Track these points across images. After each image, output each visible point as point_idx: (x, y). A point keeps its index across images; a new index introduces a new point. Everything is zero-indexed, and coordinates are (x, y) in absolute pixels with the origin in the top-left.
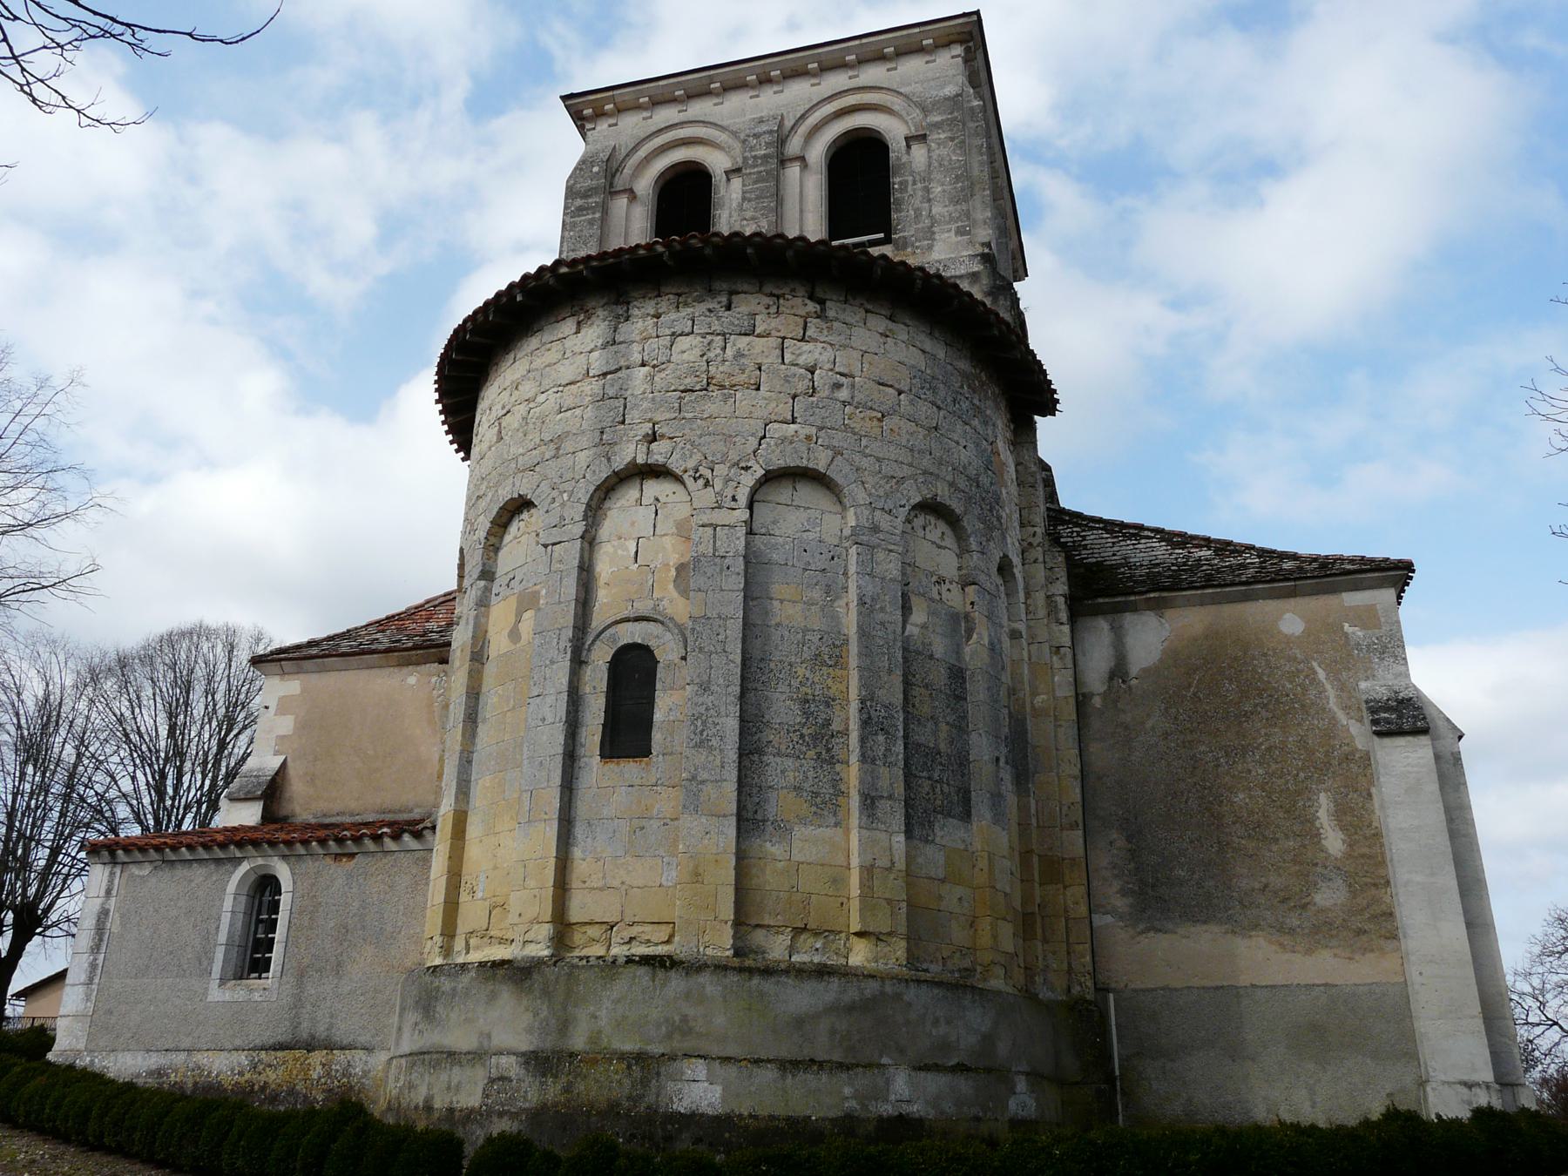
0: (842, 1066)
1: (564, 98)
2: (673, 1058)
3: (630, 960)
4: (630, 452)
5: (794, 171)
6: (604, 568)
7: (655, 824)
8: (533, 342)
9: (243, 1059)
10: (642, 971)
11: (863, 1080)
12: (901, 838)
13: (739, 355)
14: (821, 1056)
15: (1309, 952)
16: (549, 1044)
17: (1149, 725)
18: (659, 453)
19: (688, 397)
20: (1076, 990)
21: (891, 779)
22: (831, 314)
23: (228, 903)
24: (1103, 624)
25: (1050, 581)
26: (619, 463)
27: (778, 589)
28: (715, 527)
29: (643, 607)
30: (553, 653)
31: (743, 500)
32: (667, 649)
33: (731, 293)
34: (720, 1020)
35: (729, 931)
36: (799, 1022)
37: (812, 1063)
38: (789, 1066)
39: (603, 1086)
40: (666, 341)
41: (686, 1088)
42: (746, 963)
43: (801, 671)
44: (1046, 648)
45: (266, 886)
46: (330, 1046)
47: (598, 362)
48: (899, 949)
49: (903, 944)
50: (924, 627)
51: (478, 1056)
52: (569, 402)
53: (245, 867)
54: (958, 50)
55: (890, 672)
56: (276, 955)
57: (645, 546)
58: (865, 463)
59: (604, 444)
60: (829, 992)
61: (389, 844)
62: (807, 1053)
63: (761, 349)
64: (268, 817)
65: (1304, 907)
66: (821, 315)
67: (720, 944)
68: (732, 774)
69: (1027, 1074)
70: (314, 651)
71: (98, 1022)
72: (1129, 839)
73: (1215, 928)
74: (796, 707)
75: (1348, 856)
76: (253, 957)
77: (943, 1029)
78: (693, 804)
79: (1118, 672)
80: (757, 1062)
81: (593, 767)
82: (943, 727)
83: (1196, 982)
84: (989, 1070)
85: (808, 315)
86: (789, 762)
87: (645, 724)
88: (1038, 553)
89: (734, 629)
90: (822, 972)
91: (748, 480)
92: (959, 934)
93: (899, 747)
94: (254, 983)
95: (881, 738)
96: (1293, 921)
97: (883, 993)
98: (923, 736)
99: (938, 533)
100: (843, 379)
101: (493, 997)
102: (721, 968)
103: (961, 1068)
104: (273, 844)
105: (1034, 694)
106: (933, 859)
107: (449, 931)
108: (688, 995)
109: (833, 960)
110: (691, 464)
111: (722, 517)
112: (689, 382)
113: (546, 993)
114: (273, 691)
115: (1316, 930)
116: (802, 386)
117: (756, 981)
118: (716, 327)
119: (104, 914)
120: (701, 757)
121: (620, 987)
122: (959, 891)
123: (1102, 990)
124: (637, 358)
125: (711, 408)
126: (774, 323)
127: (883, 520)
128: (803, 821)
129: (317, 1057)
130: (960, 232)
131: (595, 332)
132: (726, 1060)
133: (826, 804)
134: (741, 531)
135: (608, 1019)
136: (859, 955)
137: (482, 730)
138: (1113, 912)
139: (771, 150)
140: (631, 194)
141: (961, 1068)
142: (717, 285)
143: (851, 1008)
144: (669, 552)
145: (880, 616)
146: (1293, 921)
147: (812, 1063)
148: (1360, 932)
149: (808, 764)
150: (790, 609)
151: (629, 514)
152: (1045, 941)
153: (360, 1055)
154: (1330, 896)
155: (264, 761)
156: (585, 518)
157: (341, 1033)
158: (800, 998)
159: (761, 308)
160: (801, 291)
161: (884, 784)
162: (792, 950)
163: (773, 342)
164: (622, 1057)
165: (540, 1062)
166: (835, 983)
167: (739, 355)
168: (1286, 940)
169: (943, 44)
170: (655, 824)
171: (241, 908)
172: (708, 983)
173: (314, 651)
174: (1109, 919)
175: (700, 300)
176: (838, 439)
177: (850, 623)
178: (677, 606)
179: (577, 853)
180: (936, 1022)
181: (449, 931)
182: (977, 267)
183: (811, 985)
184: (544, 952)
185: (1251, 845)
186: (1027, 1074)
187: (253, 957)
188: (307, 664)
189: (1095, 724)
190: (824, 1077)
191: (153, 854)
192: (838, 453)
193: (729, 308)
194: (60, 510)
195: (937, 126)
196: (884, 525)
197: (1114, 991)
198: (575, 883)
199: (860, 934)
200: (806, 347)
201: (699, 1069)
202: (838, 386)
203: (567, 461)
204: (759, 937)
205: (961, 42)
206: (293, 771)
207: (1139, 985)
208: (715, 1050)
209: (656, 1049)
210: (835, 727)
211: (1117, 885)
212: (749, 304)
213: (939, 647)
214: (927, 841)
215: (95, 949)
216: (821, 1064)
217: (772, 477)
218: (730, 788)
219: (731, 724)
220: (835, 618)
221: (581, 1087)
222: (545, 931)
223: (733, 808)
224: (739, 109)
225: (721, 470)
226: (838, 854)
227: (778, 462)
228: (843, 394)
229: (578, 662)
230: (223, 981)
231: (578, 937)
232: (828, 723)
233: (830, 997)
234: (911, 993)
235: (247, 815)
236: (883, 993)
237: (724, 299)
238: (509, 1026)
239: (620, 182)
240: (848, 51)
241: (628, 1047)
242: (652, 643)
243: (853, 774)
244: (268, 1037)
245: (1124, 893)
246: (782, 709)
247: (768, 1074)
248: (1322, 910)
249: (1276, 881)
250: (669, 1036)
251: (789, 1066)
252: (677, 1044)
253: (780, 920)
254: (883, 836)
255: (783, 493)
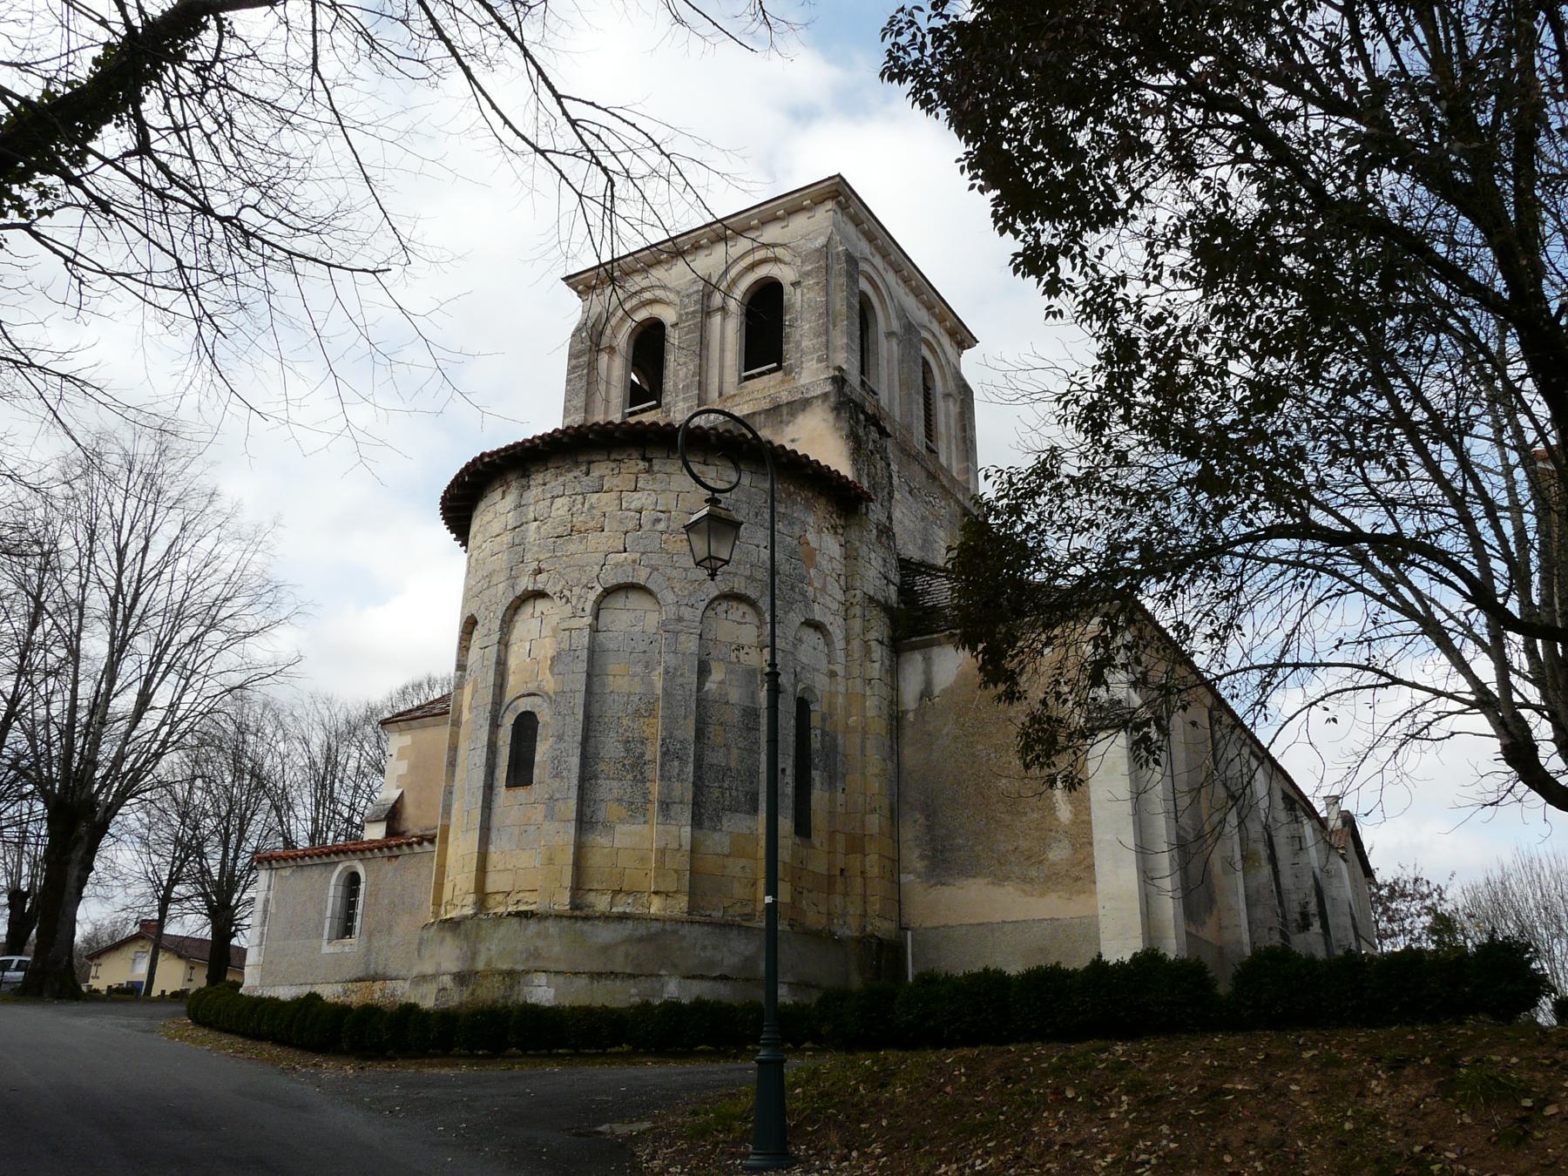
0: (632, 976)
1: (566, 279)
2: (528, 972)
3: (509, 914)
4: (525, 583)
5: (717, 319)
6: (513, 662)
7: (533, 828)
8: (482, 505)
9: (339, 988)
10: (515, 920)
11: (645, 985)
12: (689, 829)
13: (592, 507)
14: (618, 969)
15: (1042, 895)
16: (465, 968)
17: (945, 731)
18: (541, 582)
19: (560, 541)
20: (869, 929)
21: (683, 790)
22: (656, 468)
23: (331, 893)
24: (918, 657)
25: (866, 630)
26: (519, 591)
27: (612, 668)
28: (570, 630)
29: (532, 687)
30: (481, 721)
31: (589, 607)
32: (544, 716)
33: (590, 463)
34: (557, 949)
35: (568, 894)
36: (605, 949)
37: (613, 975)
38: (596, 976)
39: (490, 992)
40: (547, 503)
41: (534, 990)
42: (579, 912)
43: (625, 722)
44: (858, 681)
45: (353, 880)
46: (385, 978)
47: (511, 520)
48: (682, 903)
49: (686, 898)
50: (722, 682)
51: (434, 976)
52: (496, 550)
53: (340, 867)
54: (830, 205)
55: (685, 717)
56: (358, 924)
57: (538, 641)
58: (675, 573)
59: (513, 579)
60: (627, 929)
61: (417, 848)
62: (609, 968)
63: (606, 501)
64: (391, 832)
65: (1040, 862)
66: (649, 471)
67: (563, 902)
68: (574, 793)
69: (790, 984)
70: (418, 713)
71: (266, 969)
72: (927, 817)
73: (980, 880)
74: (621, 747)
75: (1074, 823)
76: (346, 928)
77: (709, 953)
78: (550, 815)
79: (926, 693)
80: (576, 974)
81: (502, 793)
82: (735, 751)
83: (966, 921)
84: (747, 980)
85: (640, 472)
86: (615, 783)
87: (530, 763)
88: (857, 610)
89: (580, 699)
90: (623, 917)
91: (592, 596)
92: (739, 891)
93: (690, 768)
94: (347, 941)
95: (676, 763)
96: (1033, 873)
97: (664, 930)
98: (715, 758)
99: (740, 613)
100: (662, 515)
101: (443, 940)
102: (559, 917)
103: (723, 978)
104: (354, 852)
105: (848, 716)
106: (717, 842)
107: (438, 902)
108: (538, 934)
109: (638, 910)
110: (558, 588)
111: (576, 623)
112: (560, 530)
113: (467, 937)
114: (397, 742)
115: (1048, 878)
116: (631, 525)
117: (579, 924)
118: (578, 490)
119: (267, 901)
120: (556, 784)
121: (502, 931)
122: (742, 862)
123: (903, 928)
124: (531, 516)
125: (572, 548)
126: (616, 481)
127: (687, 613)
128: (622, 821)
129: (378, 985)
130: (820, 360)
131: (511, 499)
132: (557, 973)
133: (636, 810)
134: (587, 632)
135: (498, 949)
136: (656, 906)
137: (458, 770)
138: (914, 872)
139: (698, 307)
140: (612, 350)
141: (723, 978)
142: (581, 459)
143: (641, 940)
144: (547, 649)
145: (680, 680)
146: (1033, 873)
147: (613, 975)
148: (1078, 879)
149: (627, 784)
150: (621, 682)
151: (528, 624)
152: (846, 894)
153: (400, 982)
154: (1058, 853)
155: (388, 793)
156: (501, 629)
157: (391, 972)
158: (605, 934)
159: (608, 471)
160: (635, 455)
161: (677, 794)
162: (612, 904)
163: (614, 495)
164: (501, 973)
165: (461, 978)
166: (630, 923)
167: (592, 507)
168: (1027, 887)
169: (818, 201)
170: (533, 828)
171: (340, 894)
172: (551, 927)
173: (418, 713)
174: (912, 877)
175: (569, 471)
176: (655, 559)
177: (659, 685)
178: (549, 683)
179: (492, 848)
180: (704, 948)
181: (438, 902)
182: (828, 388)
183: (612, 926)
184: (469, 911)
185: (1008, 818)
186: (790, 984)
187: (346, 928)
188: (414, 723)
189: (908, 733)
190: (618, 983)
191: (291, 863)
192: (654, 569)
193: (587, 474)
194: (276, 618)
195: (808, 274)
196: (686, 616)
197: (913, 929)
198: (490, 868)
199: (656, 893)
200: (636, 495)
201: (542, 979)
202: (658, 520)
203: (493, 590)
204: (591, 897)
205: (833, 198)
206: (408, 800)
207: (928, 925)
208: (553, 967)
209: (520, 967)
210: (647, 757)
211: (917, 853)
212: (601, 469)
213: (735, 695)
214: (715, 830)
215: (263, 924)
216: (616, 975)
217: (609, 592)
218: (573, 804)
219: (575, 761)
220: (651, 684)
221: (479, 992)
222: (471, 899)
223: (574, 815)
224: (677, 275)
225: (576, 590)
226: (643, 843)
227: (612, 581)
228: (661, 526)
229: (495, 725)
230: (330, 940)
231: (491, 902)
232: (642, 755)
233: (626, 933)
234: (685, 930)
235: (376, 832)
236: (664, 930)
237: (584, 468)
238: (447, 957)
239: (605, 342)
240: (752, 217)
241: (505, 967)
242: (536, 711)
243: (655, 789)
244: (353, 974)
245: (922, 857)
246: (611, 747)
247: (582, 981)
248: (1053, 864)
249: (1024, 844)
250: (527, 959)
251: (596, 976)
252: (532, 964)
253: (604, 886)
254: (674, 829)
255: (619, 601)
